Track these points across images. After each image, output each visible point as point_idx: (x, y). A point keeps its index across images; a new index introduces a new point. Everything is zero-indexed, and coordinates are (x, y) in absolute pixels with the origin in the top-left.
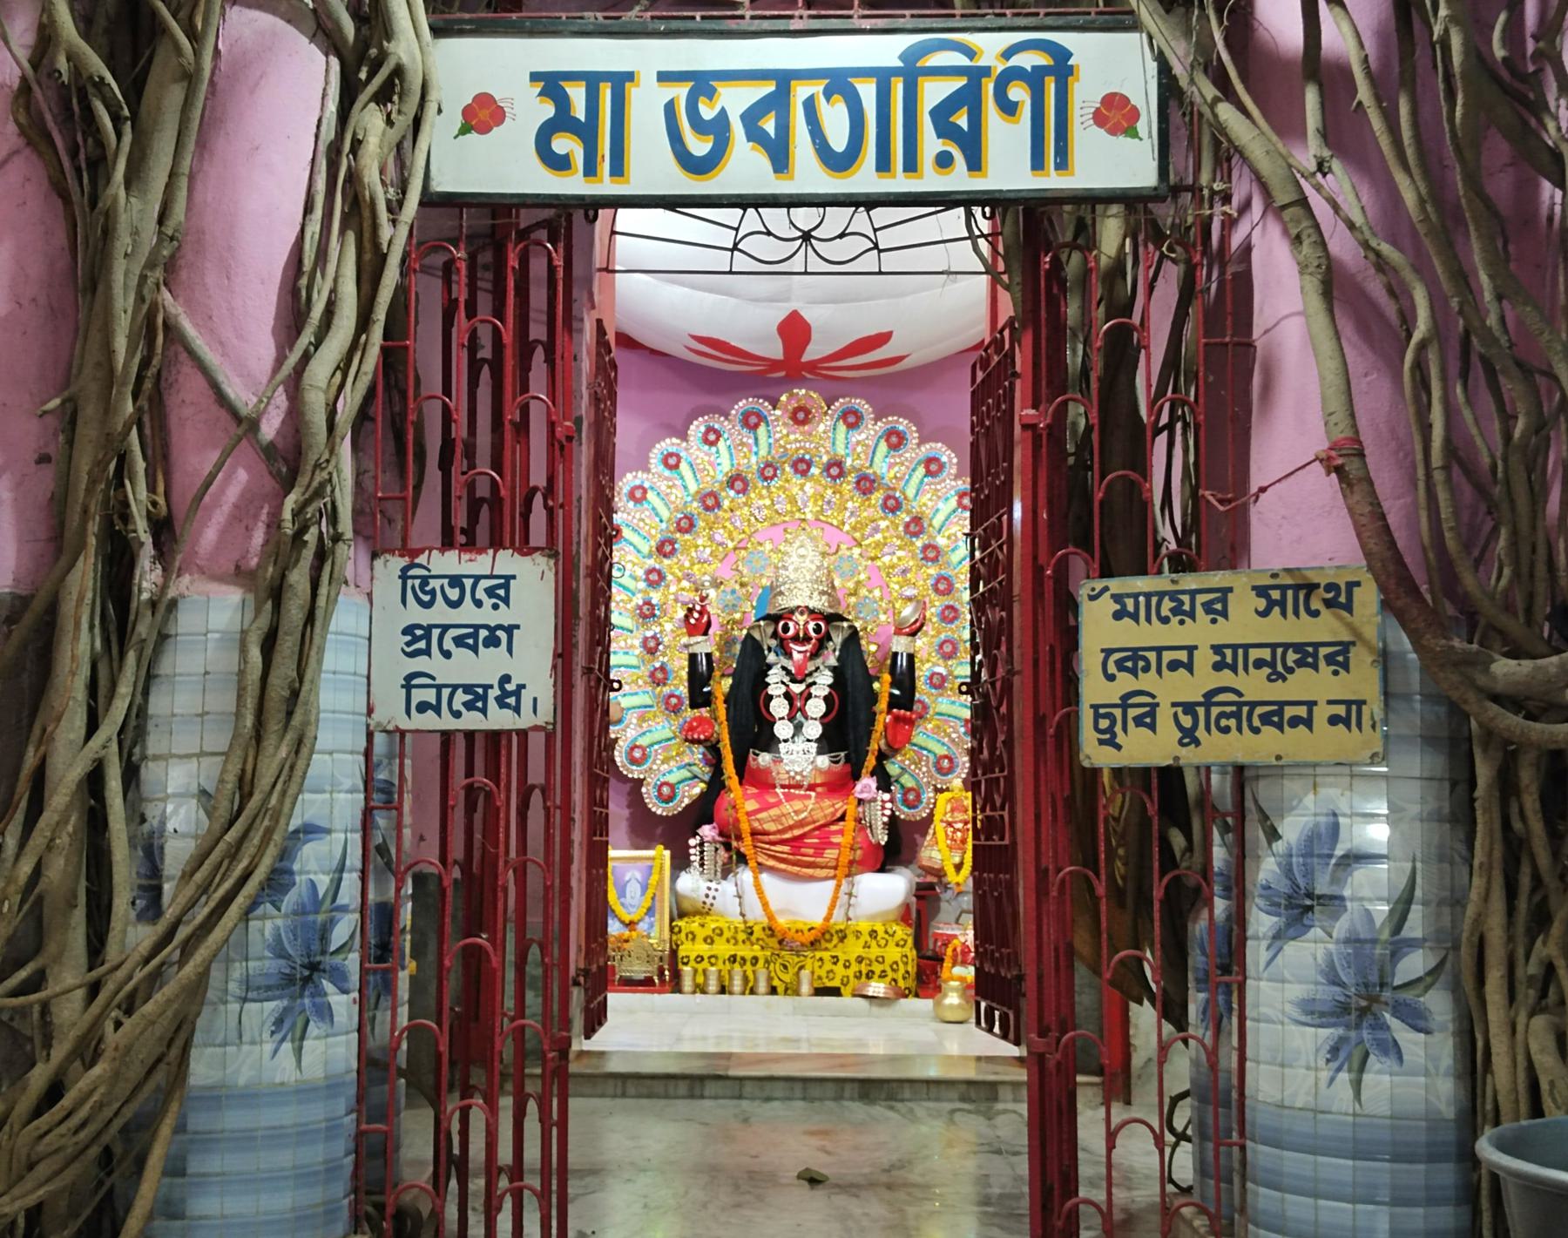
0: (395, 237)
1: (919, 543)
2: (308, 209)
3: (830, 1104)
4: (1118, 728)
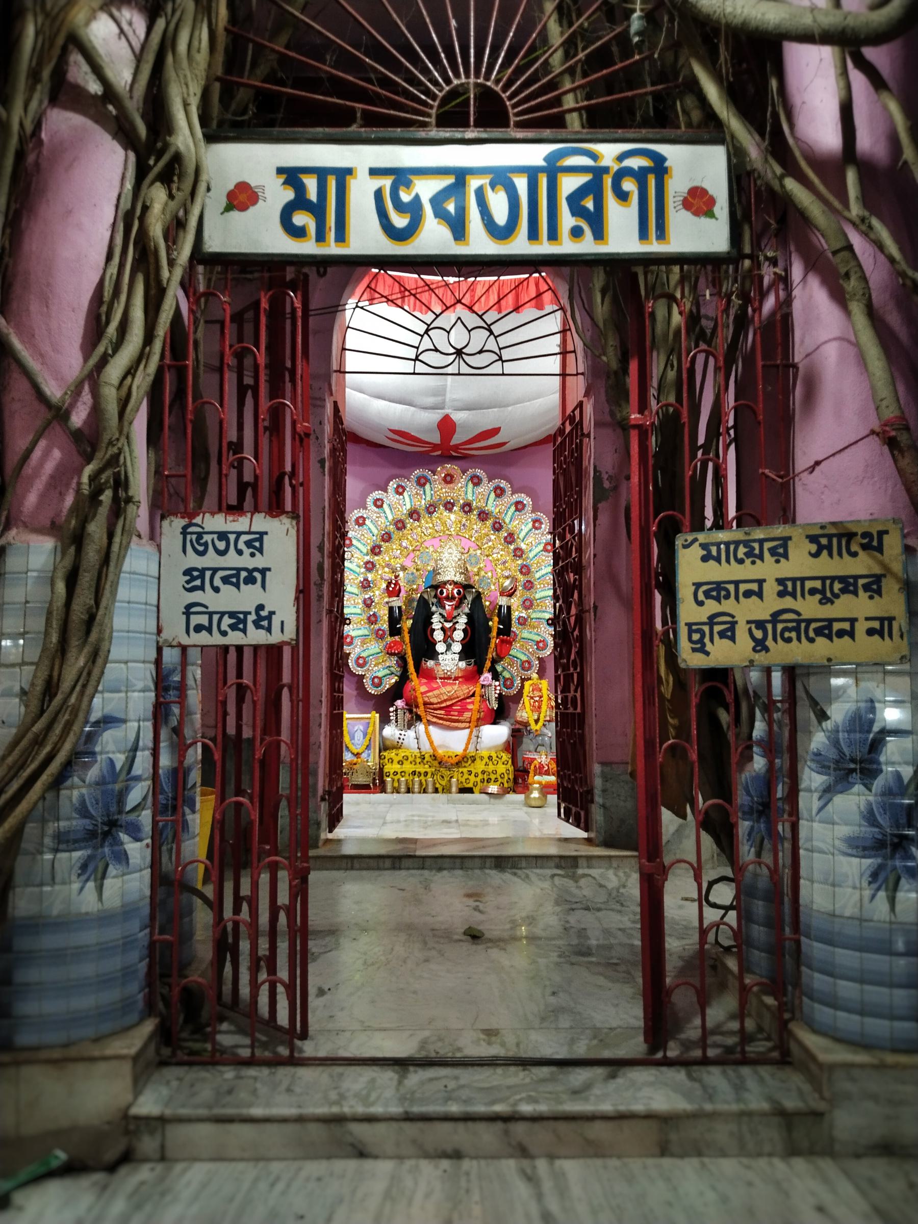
0: (172, 278)
1: (512, 547)
2: (109, 257)
3: (477, 871)
4: (707, 640)
